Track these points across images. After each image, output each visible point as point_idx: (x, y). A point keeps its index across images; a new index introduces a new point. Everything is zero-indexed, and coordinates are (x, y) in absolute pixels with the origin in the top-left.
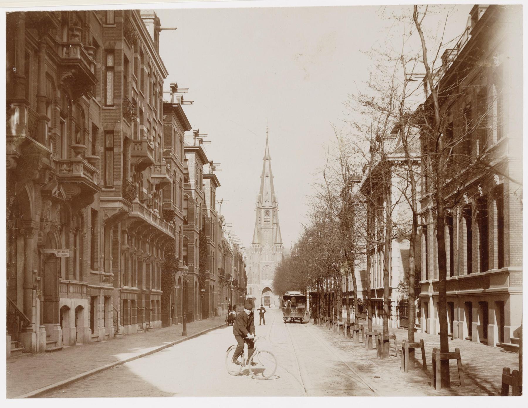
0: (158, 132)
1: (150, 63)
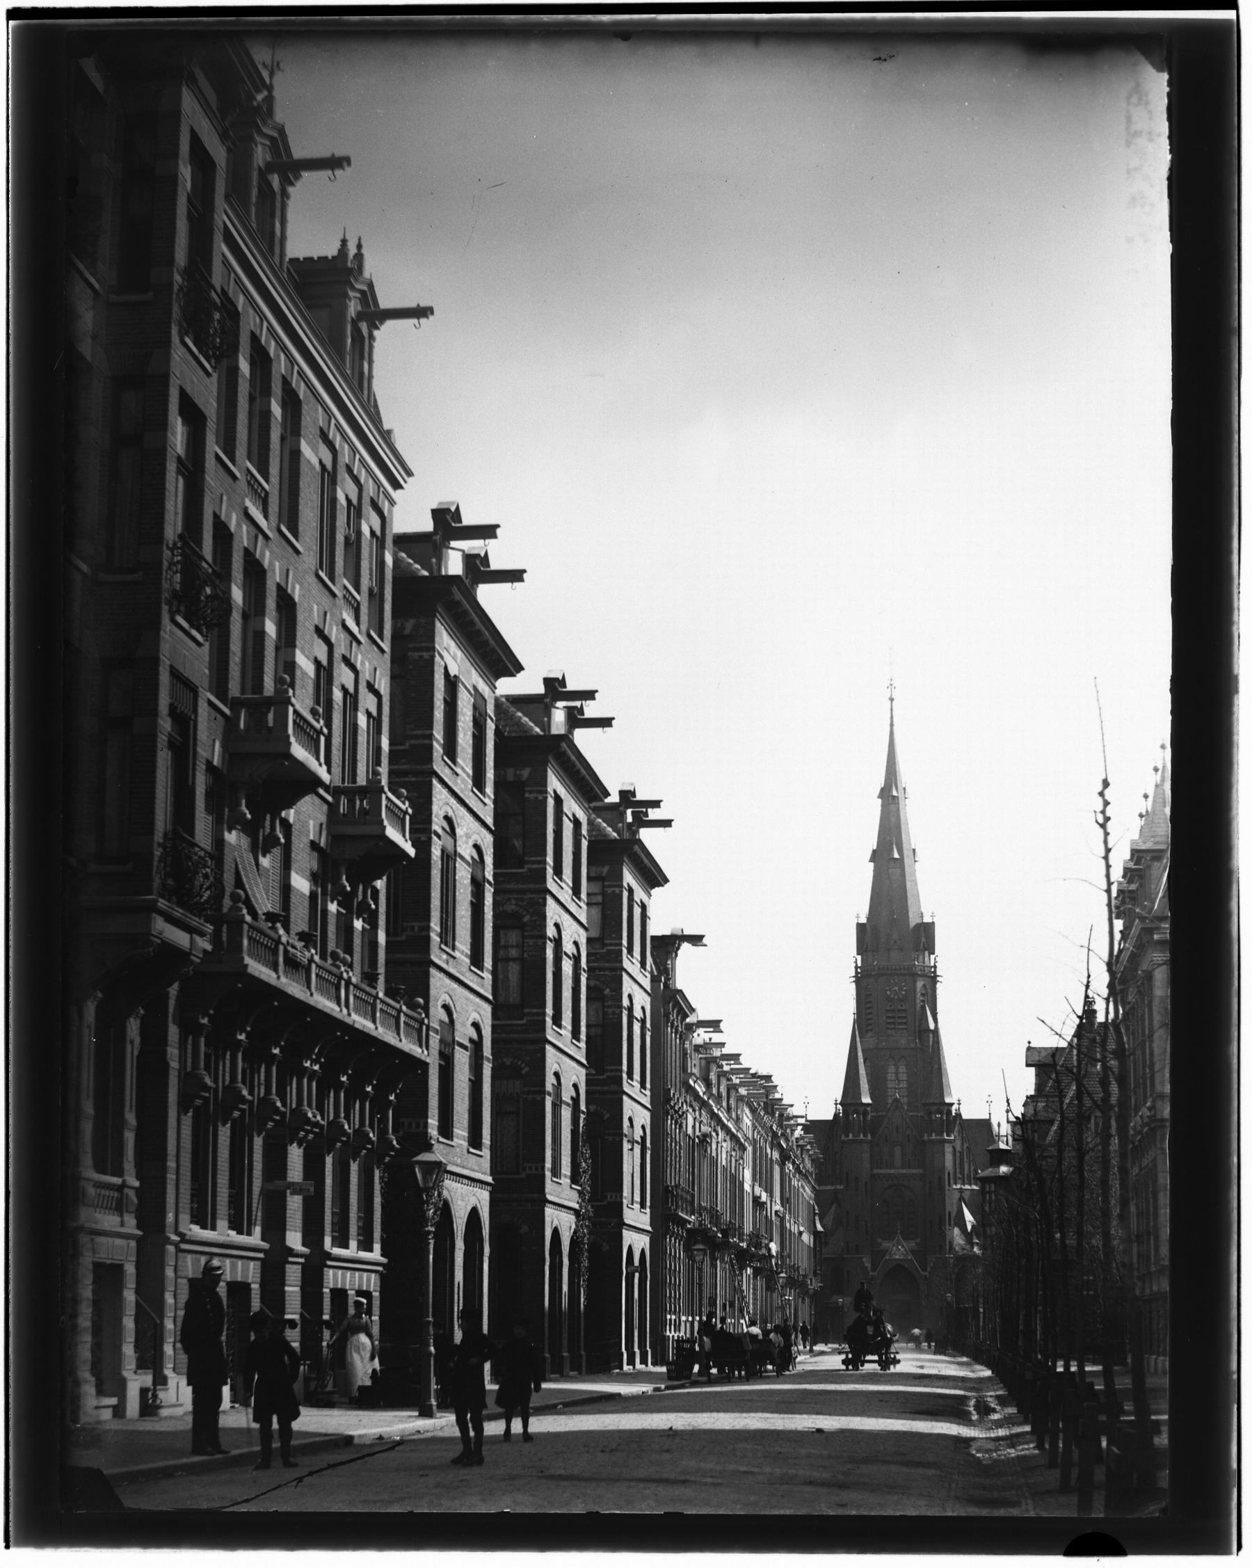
0: (366, 675)
1: (332, 433)
